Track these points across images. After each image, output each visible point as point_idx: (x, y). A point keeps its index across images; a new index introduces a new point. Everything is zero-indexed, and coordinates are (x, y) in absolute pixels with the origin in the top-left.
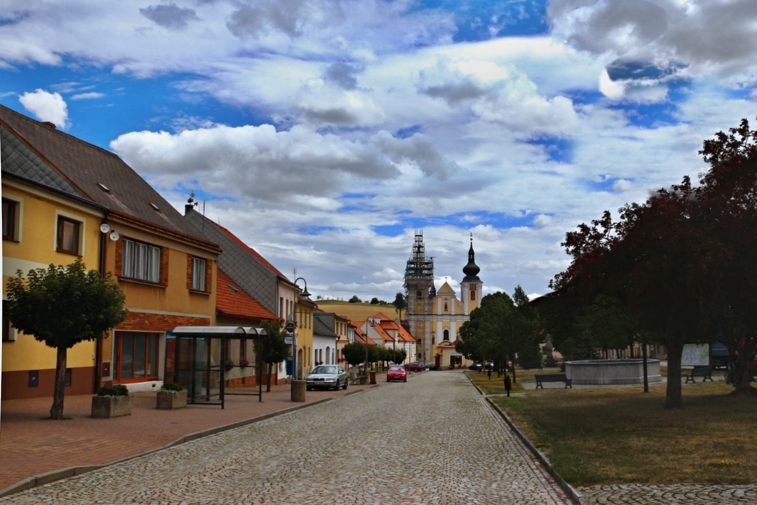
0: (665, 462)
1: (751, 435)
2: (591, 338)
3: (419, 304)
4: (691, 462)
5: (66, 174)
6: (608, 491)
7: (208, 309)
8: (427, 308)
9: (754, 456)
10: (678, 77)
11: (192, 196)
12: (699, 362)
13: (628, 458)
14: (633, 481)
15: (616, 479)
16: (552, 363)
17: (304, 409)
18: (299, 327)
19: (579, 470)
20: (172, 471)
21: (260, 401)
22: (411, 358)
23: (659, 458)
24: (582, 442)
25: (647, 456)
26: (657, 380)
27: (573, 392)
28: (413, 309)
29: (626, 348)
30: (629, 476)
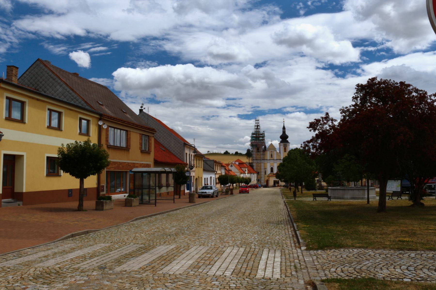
0: (376, 239)
1: (420, 227)
2: (341, 176)
3: (258, 154)
4: (389, 239)
5: (83, 97)
6: (347, 252)
7: (150, 159)
8: (262, 157)
9: (421, 237)
10: (386, 46)
11: (143, 105)
12: (395, 189)
13: (358, 236)
14: (360, 247)
15: (351, 246)
16: (321, 188)
17: (195, 206)
18: (195, 167)
19: (333, 241)
20: (129, 232)
21: (174, 202)
22: (254, 181)
23: (373, 237)
24: (335, 228)
25: (368, 235)
26: (374, 198)
27: (331, 203)
28: (255, 157)
29: (359, 181)
30: (358, 245)
